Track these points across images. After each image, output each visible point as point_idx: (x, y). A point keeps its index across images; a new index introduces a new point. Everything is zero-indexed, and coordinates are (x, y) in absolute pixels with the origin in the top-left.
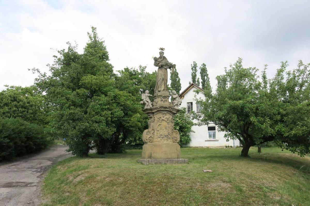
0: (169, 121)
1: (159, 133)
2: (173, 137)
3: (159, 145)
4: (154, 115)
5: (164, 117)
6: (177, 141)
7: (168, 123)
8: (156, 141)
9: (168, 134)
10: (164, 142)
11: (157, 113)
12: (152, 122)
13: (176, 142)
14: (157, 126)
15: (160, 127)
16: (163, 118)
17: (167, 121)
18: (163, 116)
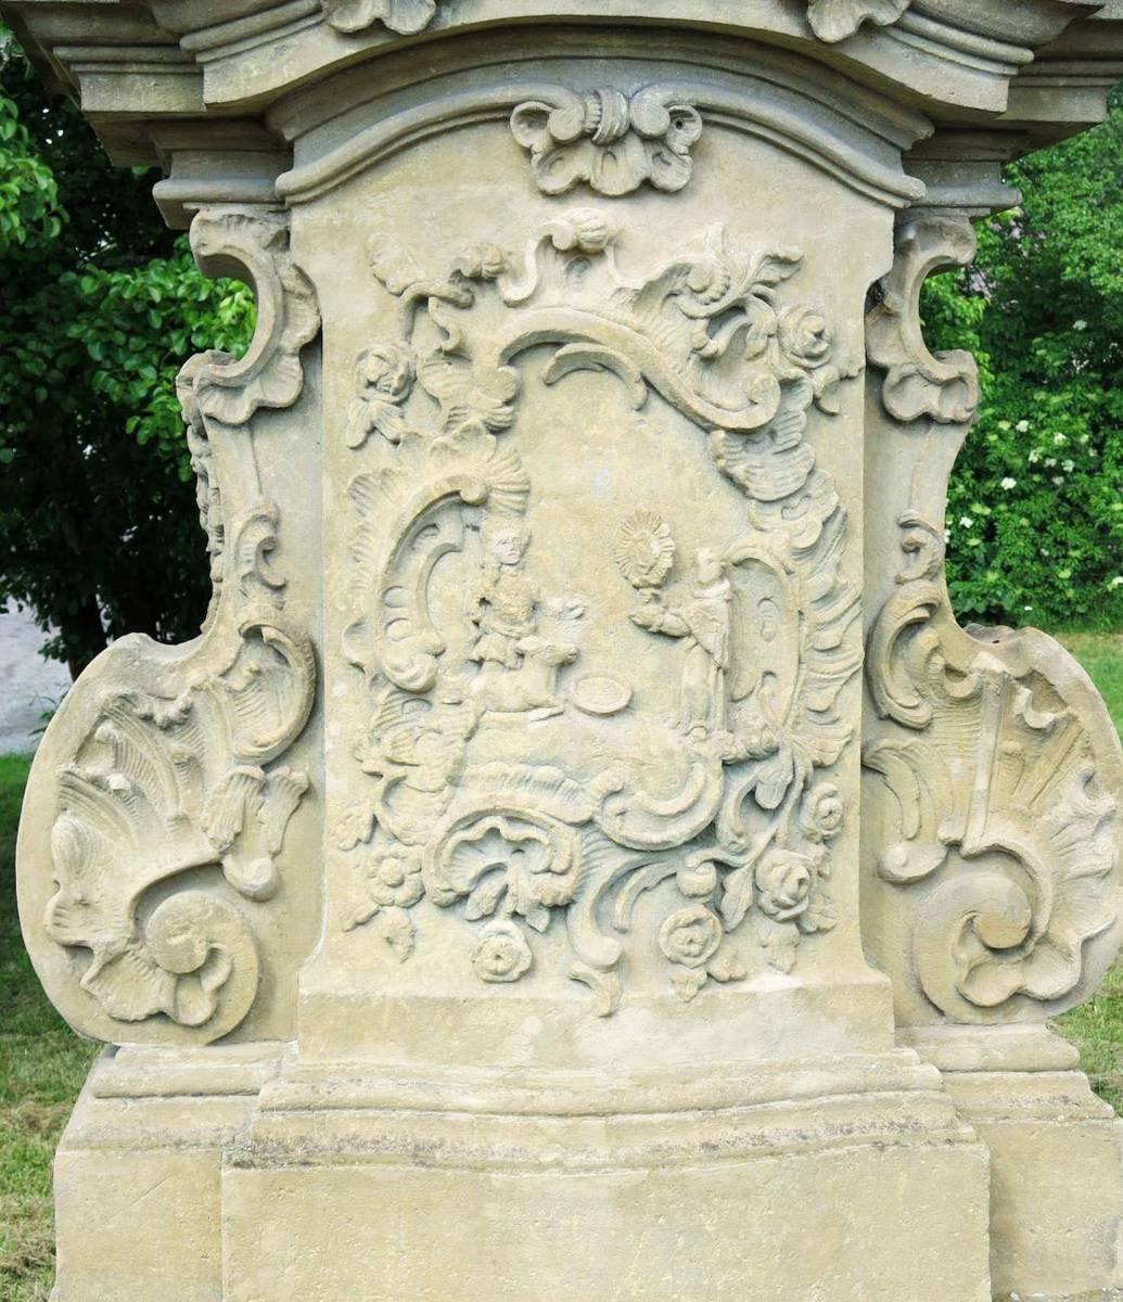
0: (759, 375)
1: (430, 756)
2: (902, 858)
3: (420, 1156)
4: (282, 205)
5: (581, 255)
6: (1049, 979)
7: (746, 435)
8: (353, 1019)
9: (709, 792)
10: (598, 1040)
11: (393, 124)
12: (241, 410)
13: (1018, 995)
14: (381, 548)
15: (457, 584)
16: (586, 304)
17: (683, 378)
18: (581, 219)
